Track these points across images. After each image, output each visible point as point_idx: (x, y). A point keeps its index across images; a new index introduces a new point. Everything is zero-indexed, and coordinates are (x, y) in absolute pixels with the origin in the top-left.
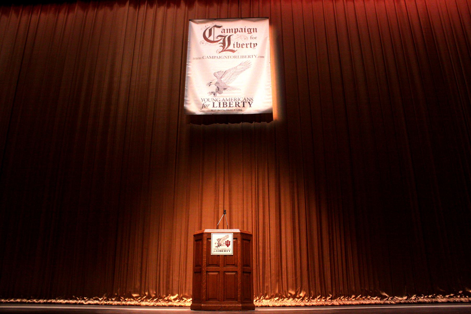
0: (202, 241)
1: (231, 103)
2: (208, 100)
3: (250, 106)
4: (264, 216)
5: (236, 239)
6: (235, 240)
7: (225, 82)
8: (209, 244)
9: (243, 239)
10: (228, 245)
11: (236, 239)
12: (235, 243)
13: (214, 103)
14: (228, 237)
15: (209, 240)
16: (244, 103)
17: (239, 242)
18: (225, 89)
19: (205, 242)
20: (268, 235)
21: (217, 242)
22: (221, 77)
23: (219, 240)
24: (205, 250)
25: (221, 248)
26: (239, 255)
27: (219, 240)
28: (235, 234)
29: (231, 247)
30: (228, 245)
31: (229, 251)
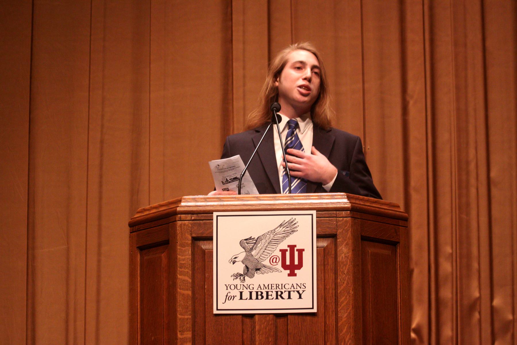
0: (166, 246)
1: (270, 293)
2: (236, 287)
3: (300, 297)
4: (461, 131)
5: (333, 236)
6: (324, 243)
7: (256, 257)
8: (203, 264)
9: (364, 238)
10: (292, 269)
11: (333, 236)
12: (326, 260)
13: (241, 293)
14: (290, 228)
15: (204, 245)
16: (289, 292)
17: (345, 251)
18: (258, 270)
19: (184, 255)
20: (484, 219)
21: (242, 255)
22: (252, 249)
23: (249, 244)
24: (184, 292)
25: (258, 281)
26: (346, 313)
27: (249, 244)
28: (322, 212)
29: (307, 275)
30: (292, 269)
31: (301, 292)
